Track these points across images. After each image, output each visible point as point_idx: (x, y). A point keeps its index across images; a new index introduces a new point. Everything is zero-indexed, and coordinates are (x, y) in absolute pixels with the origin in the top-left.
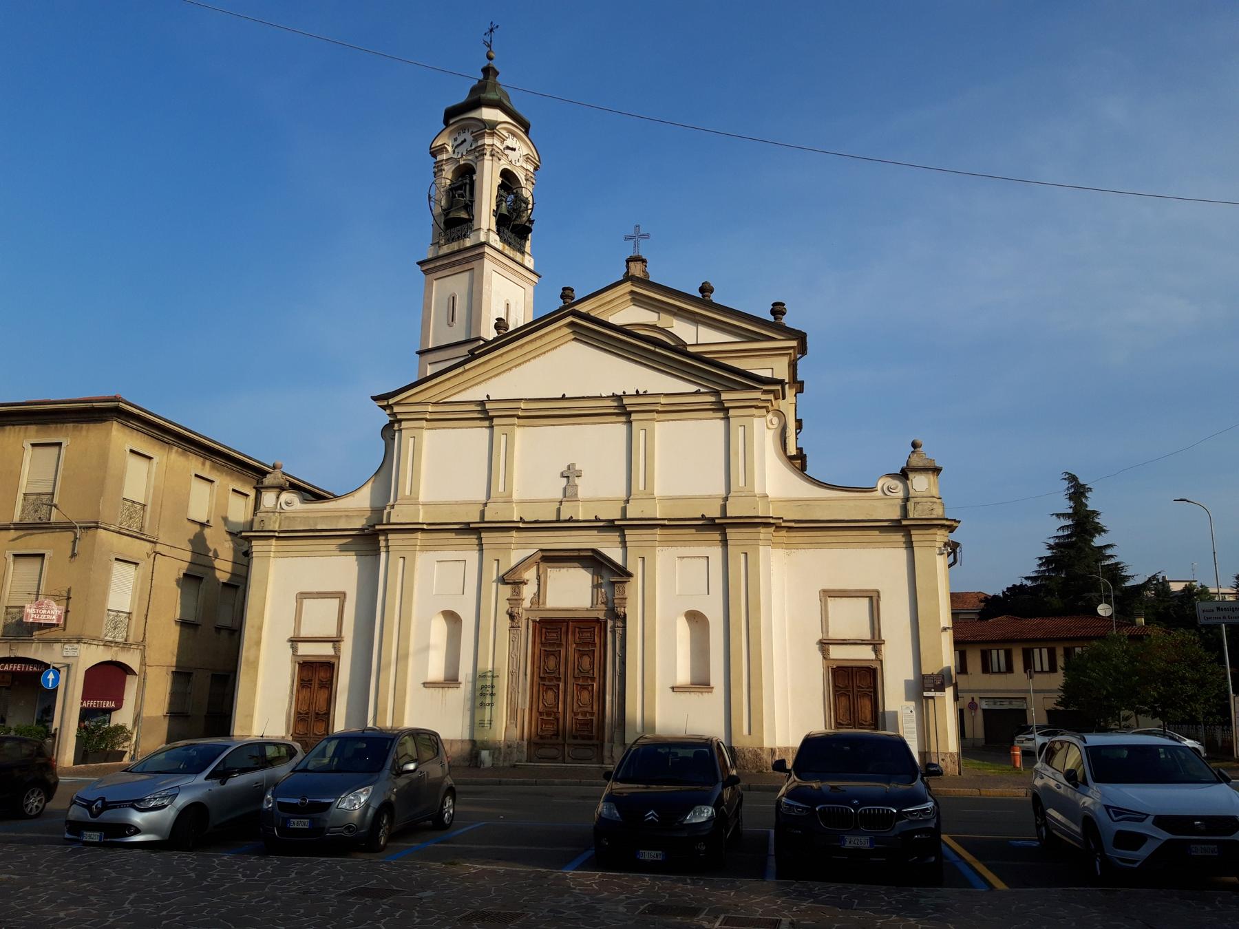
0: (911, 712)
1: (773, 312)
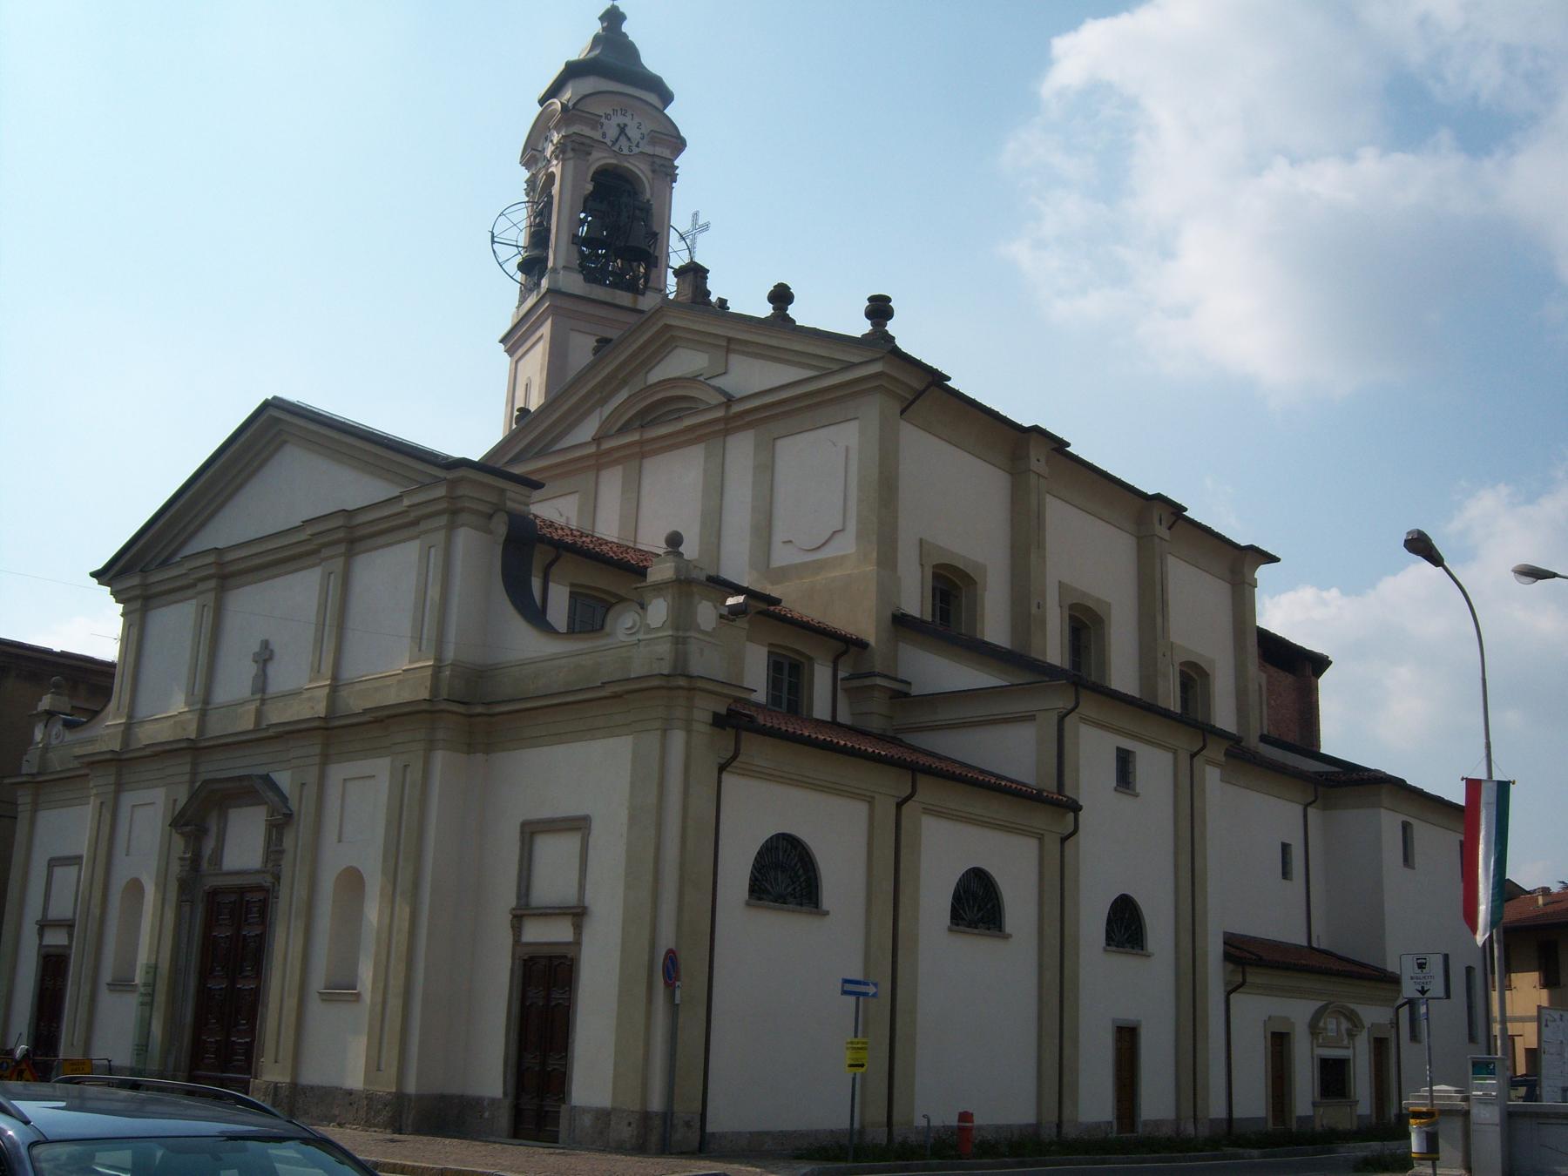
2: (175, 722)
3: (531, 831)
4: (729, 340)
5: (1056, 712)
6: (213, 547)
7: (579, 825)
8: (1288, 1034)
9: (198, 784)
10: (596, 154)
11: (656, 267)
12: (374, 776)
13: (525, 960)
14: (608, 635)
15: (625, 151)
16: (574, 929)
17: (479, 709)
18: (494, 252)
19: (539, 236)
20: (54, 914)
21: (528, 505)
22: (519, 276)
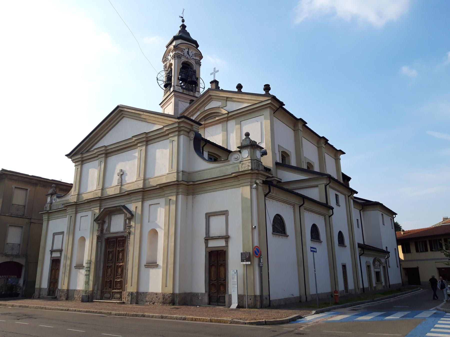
0: (235, 273)
1: (237, 87)
2: (94, 193)
3: (208, 216)
4: (227, 98)
5: (324, 184)
6: (104, 145)
7: (225, 213)
8: (370, 266)
9: (102, 210)
10: (182, 58)
11: (198, 86)
12: (159, 203)
13: (209, 252)
14: (229, 161)
15: (189, 58)
16: (226, 242)
17: (191, 183)
18: (158, 82)
19: (169, 78)
20: (55, 248)
21: (198, 130)
22: (164, 88)
